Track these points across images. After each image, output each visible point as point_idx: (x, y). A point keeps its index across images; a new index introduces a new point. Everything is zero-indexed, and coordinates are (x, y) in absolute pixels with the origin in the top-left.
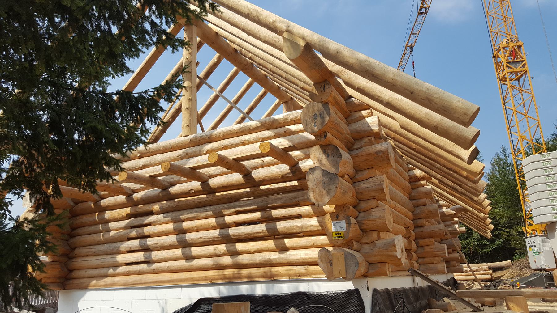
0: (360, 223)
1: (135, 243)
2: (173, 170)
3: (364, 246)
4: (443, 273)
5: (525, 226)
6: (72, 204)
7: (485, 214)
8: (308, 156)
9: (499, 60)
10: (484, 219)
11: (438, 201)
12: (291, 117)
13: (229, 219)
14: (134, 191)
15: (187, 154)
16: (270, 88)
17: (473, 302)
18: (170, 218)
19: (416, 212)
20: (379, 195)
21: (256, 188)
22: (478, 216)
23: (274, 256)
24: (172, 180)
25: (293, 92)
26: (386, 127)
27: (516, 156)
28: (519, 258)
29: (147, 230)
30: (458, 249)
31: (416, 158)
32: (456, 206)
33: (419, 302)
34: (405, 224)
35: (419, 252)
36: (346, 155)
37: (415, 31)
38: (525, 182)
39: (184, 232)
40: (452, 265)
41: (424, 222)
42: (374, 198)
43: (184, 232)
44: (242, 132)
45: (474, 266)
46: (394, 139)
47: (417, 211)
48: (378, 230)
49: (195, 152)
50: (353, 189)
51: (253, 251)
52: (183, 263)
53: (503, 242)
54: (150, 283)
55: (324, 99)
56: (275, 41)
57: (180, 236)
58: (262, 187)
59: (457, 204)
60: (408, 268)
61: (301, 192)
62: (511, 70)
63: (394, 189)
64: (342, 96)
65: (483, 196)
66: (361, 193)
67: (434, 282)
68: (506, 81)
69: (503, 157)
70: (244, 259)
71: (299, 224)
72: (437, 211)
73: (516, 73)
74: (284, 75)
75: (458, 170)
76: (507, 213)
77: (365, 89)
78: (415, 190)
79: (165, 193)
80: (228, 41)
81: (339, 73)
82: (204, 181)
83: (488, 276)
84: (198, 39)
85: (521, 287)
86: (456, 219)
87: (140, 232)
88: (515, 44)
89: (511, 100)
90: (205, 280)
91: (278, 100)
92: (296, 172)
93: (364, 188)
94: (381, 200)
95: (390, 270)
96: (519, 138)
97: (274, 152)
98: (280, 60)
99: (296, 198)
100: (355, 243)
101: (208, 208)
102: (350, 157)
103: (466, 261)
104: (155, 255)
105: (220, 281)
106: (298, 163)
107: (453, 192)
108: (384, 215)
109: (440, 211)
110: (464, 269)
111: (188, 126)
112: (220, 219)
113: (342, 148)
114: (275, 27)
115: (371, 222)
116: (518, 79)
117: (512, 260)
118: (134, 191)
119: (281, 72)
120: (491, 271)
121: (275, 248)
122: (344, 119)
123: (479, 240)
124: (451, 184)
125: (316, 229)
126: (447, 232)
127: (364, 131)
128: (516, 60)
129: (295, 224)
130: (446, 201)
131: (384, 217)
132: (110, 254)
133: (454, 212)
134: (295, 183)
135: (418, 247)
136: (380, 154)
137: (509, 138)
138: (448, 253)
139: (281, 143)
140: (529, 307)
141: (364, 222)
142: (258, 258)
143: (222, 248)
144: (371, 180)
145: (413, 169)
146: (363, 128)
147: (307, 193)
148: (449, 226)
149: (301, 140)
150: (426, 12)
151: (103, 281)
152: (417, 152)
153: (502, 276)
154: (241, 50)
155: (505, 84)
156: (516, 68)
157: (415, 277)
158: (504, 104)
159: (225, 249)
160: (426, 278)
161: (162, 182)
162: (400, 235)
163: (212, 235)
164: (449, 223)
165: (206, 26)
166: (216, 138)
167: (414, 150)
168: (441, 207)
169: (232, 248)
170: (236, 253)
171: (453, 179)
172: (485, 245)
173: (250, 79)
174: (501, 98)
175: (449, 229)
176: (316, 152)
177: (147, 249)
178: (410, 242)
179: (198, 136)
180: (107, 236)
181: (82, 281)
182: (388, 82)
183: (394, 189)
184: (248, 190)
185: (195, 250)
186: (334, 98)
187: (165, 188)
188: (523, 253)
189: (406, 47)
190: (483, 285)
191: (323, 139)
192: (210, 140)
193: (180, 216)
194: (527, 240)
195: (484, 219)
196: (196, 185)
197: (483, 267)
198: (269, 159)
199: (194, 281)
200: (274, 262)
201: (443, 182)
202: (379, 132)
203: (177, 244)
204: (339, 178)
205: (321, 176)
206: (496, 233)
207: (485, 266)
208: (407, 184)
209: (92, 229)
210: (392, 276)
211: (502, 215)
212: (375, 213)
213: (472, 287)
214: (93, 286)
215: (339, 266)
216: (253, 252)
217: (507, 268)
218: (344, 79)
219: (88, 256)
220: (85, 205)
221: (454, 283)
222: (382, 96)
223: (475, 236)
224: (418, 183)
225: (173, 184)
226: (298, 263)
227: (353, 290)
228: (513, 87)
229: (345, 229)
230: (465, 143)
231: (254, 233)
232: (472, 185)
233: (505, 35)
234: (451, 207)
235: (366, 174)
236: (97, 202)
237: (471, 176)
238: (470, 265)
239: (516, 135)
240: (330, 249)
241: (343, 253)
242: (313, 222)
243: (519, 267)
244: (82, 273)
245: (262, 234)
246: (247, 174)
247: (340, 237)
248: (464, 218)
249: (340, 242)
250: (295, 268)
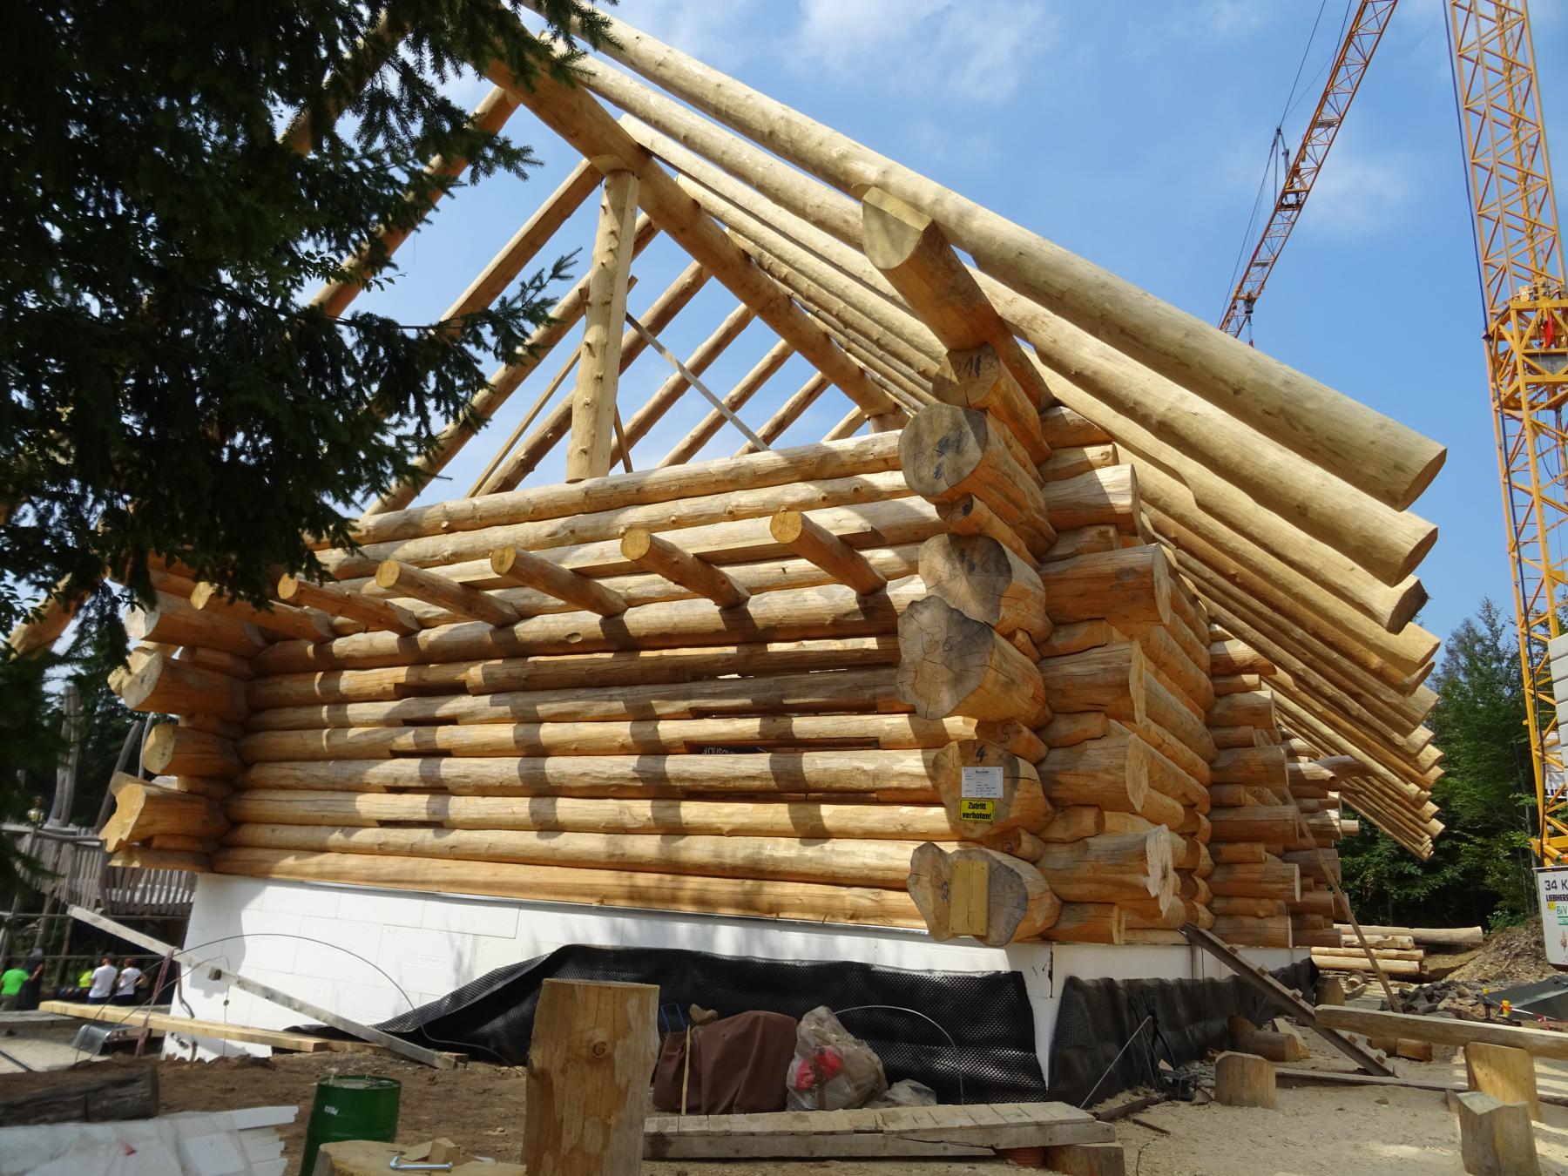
0: (1048, 782)
1: (410, 768)
2: (523, 571)
3: (1054, 848)
4: (1281, 945)
5: (1537, 832)
6: (259, 642)
7: (1423, 788)
8: (912, 569)
9: (1502, 347)
10: (1419, 802)
11: (1287, 737)
12: (878, 448)
13: (669, 730)
14: (424, 624)
15: (573, 532)
16: (837, 373)
17: (1361, 1044)
18: (507, 708)
19: (1220, 764)
20: (1113, 701)
21: (757, 649)
22: (1399, 792)
23: (785, 850)
24: (526, 602)
25: (900, 386)
26: (1154, 502)
27: (1529, 629)
28: (1509, 923)
29: (444, 736)
30: (1332, 880)
31: (1235, 605)
32: (1339, 757)
33: (1201, 1025)
34: (1184, 795)
35: (1218, 877)
36: (1024, 573)
37: (1264, 255)
38: (1552, 707)
39: (541, 751)
40: (1309, 924)
41: (1243, 793)
42: (1097, 709)
43: (541, 751)
44: (731, 481)
45: (1373, 933)
46: (1175, 541)
47: (1225, 759)
48: (1099, 806)
49: (596, 528)
50: (1038, 677)
51: (727, 828)
52: (529, 840)
53: (1463, 874)
54: (438, 883)
55: (976, 397)
56: (847, 222)
57: (531, 762)
58: (775, 647)
59: (1343, 752)
60: (1179, 923)
61: (886, 671)
62: (1537, 379)
63: (1163, 690)
64: (1030, 397)
65: (1422, 734)
66: (1063, 692)
67: (1251, 971)
68: (1519, 408)
69: (1483, 630)
70: (698, 849)
71: (869, 767)
72: (1281, 765)
73: (1553, 387)
74: (876, 331)
75: (1357, 648)
76: (1482, 793)
77: (1099, 378)
78: (1225, 701)
79: (502, 636)
80: (727, 230)
81: (1024, 326)
82: (612, 612)
83: (1412, 966)
84: (642, 218)
85: (1514, 1020)
86: (1335, 795)
87: (426, 738)
88: (1555, 302)
89: (1531, 466)
90: (586, 895)
91: (857, 409)
92: (875, 612)
93: (1072, 676)
94: (1118, 718)
95: (1123, 926)
96: (1544, 575)
97: (811, 543)
98: (856, 279)
99: (868, 687)
100: (1025, 838)
101: (616, 691)
102: (1037, 579)
103: (1351, 916)
104: (461, 807)
105: (621, 904)
106: (884, 585)
107: (1333, 716)
108: (1121, 761)
109: (1290, 766)
110: (1345, 938)
111: (584, 452)
112: (645, 728)
113: (1017, 552)
114: (846, 173)
115: (1082, 781)
116: (1556, 407)
117: (1486, 927)
118: (424, 624)
119: (866, 323)
120: (1420, 953)
121: (791, 827)
122: (1030, 465)
123: (1394, 860)
124: (1329, 689)
125: (916, 784)
126: (1305, 828)
127: (1089, 506)
128: (1553, 349)
129: (856, 764)
130: (1310, 739)
131: (1122, 768)
132: (342, 790)
133: (1330, 774)
134: (871, 643)
135: (1217, 863)
136: (1129, 580)
137: (1512, 575)
138: (1304, 889)
139: (839, 521)
140: (1539, 1081)
141: (1062, 778)
142: (738, 850)
143: (642, 809)
144: (1095, 654)
145: (1225, 638)
146: (1086, 496)
147: (894, 677)
148: (1311, 812)
149: (901, 519)
150: (1298, 206)
151: (313, 862)
152: (1241, 586)
153: (1452, 970)
154: (761, 255)
155: (1513, 417)
156: (1553, 372)
157: (1199, 951)
158: (1508, 474)
159: (650, 814)
160: (1228, 957)
161: (498, 605)
162: (1164, 827)
163: (617, 771)
164: (1312, 803)
165: (668, 180)
166: (657, 492)
167: (1232, 578)
168: (1293, 754)
169: (668, 814)
170: (679, 830)
171: (1338, 676)
172: (1410, 876)
173: (782, 342)
174: (1499, 456)
175: (1312, 821)
176: (933, 555)
177: (437, 788)
178: (1193, 849)
179: (609, 483)
180: (336, 741)
181: (260, 854)
182: (1166, 354)
183: (1163, 690)
184: (732, 650)
185: (566, 808)
186: (1007, 400)
187: (504, 622)
188: (1525, 906)
189: (1234, 300)
190: (1395, 991)
191: (959, 517)
192: (639, 496)
193: (535, 704)
194: (1542, 879)
195: (1419, 802)
196: (588, 621)
197: (1399, 938)
198: (800, 565)
199: (556, 894)
200: (785, 867)
201: (1308, 684)
202: (1130, 514)
203: (520, 783)
204: (997, 636)
205: (943, 624)
206: (1445, 844)
207: (1405, 935)
208: (1204, 679)
209: (303, 714)
210: (1129, 943)
211: (1469, 796)
212: (1096, 754)
213: (1362, 991)
214: (289, 873)
215: (970, 898)
216: (725, 831)
217: (1470, 949)
218: (1038, 342)
219: (283, 788)
220: (292, 647)
221: (1310, 978)
222: (1148, 401)
223: (1382, 846)
224: (1235, 680)
225: (526, 615)
226: (853, 878)
227: (1007, 974)
228: (1537, 428)
229: (999, 792)
230: (1388, 567)
231: (736, 778)
232: (1393, 697)
233: (1527, 275)
234: (1323, 757)
235: (1082, 634)
236: (322, 643)
237: (1394, 671)
238: (1363, 928)
239: (1535, 568)
240: (950, 848)
241: (985, 864)
242: (912, 763)
243: (1505, 952)
244: (265, 833)
245: (757, 783)
246: (733, 604)
247: (984, 816)
248: (1357, 793)
249: (980, 830)
250: (843, 891)
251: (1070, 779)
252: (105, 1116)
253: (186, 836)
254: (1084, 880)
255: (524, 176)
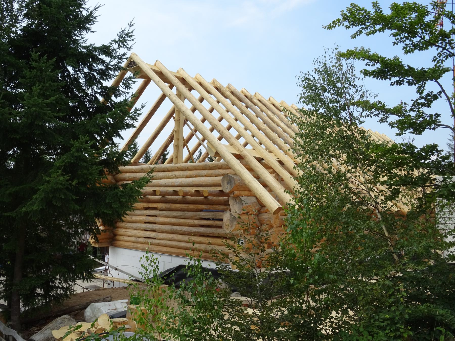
219: (124, 228)
244: (121, 238)
252: (106, 301)
253: (106, 239)
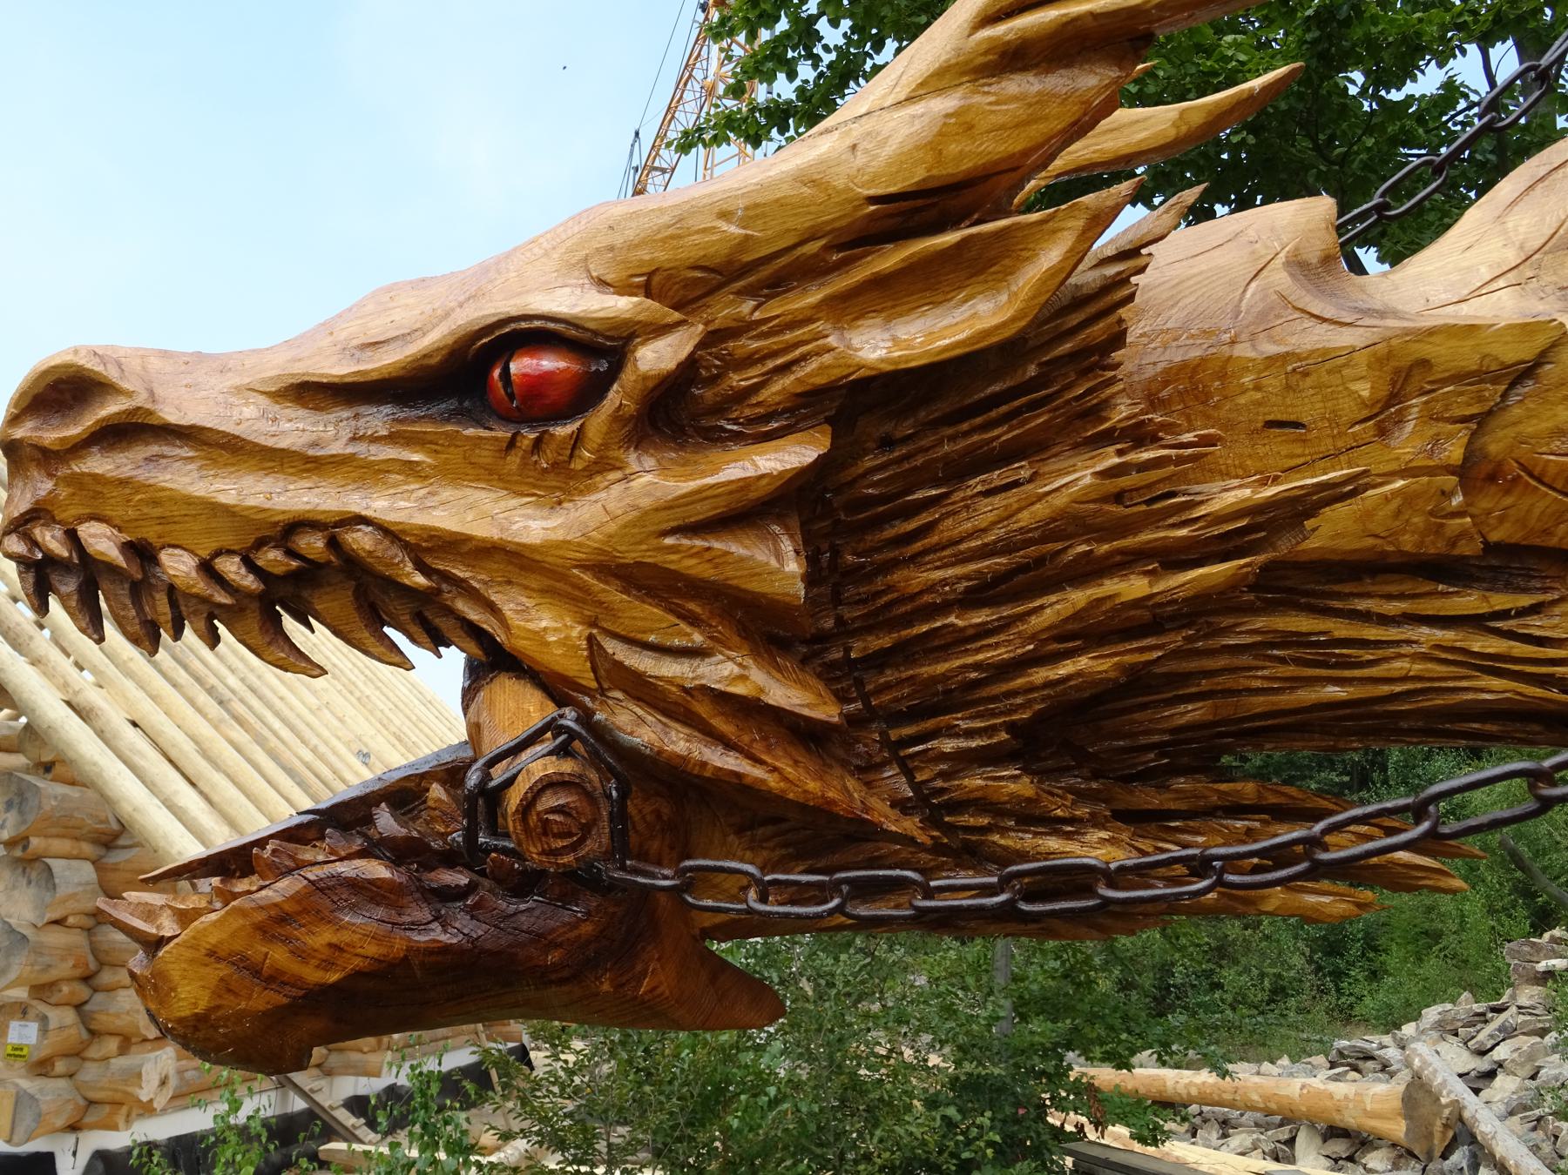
251: (103, 1018)
254: (102, 1089)
255: (440, 656)
